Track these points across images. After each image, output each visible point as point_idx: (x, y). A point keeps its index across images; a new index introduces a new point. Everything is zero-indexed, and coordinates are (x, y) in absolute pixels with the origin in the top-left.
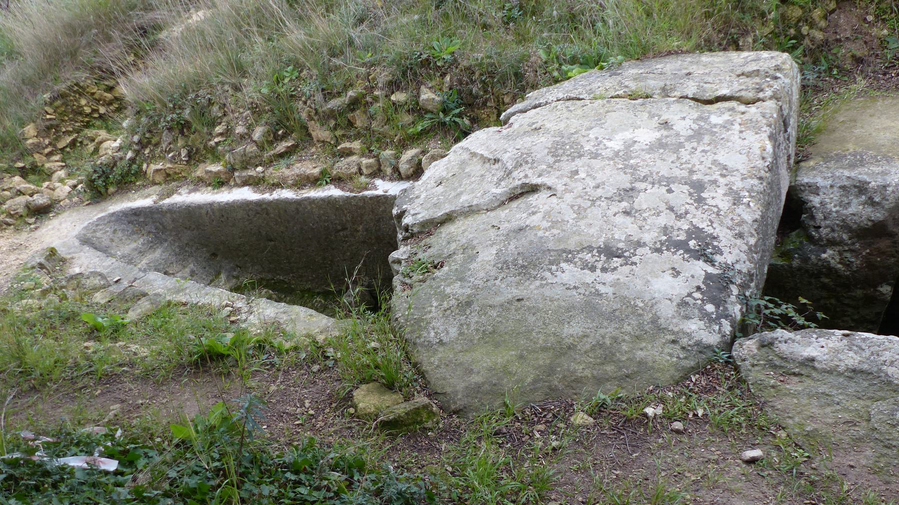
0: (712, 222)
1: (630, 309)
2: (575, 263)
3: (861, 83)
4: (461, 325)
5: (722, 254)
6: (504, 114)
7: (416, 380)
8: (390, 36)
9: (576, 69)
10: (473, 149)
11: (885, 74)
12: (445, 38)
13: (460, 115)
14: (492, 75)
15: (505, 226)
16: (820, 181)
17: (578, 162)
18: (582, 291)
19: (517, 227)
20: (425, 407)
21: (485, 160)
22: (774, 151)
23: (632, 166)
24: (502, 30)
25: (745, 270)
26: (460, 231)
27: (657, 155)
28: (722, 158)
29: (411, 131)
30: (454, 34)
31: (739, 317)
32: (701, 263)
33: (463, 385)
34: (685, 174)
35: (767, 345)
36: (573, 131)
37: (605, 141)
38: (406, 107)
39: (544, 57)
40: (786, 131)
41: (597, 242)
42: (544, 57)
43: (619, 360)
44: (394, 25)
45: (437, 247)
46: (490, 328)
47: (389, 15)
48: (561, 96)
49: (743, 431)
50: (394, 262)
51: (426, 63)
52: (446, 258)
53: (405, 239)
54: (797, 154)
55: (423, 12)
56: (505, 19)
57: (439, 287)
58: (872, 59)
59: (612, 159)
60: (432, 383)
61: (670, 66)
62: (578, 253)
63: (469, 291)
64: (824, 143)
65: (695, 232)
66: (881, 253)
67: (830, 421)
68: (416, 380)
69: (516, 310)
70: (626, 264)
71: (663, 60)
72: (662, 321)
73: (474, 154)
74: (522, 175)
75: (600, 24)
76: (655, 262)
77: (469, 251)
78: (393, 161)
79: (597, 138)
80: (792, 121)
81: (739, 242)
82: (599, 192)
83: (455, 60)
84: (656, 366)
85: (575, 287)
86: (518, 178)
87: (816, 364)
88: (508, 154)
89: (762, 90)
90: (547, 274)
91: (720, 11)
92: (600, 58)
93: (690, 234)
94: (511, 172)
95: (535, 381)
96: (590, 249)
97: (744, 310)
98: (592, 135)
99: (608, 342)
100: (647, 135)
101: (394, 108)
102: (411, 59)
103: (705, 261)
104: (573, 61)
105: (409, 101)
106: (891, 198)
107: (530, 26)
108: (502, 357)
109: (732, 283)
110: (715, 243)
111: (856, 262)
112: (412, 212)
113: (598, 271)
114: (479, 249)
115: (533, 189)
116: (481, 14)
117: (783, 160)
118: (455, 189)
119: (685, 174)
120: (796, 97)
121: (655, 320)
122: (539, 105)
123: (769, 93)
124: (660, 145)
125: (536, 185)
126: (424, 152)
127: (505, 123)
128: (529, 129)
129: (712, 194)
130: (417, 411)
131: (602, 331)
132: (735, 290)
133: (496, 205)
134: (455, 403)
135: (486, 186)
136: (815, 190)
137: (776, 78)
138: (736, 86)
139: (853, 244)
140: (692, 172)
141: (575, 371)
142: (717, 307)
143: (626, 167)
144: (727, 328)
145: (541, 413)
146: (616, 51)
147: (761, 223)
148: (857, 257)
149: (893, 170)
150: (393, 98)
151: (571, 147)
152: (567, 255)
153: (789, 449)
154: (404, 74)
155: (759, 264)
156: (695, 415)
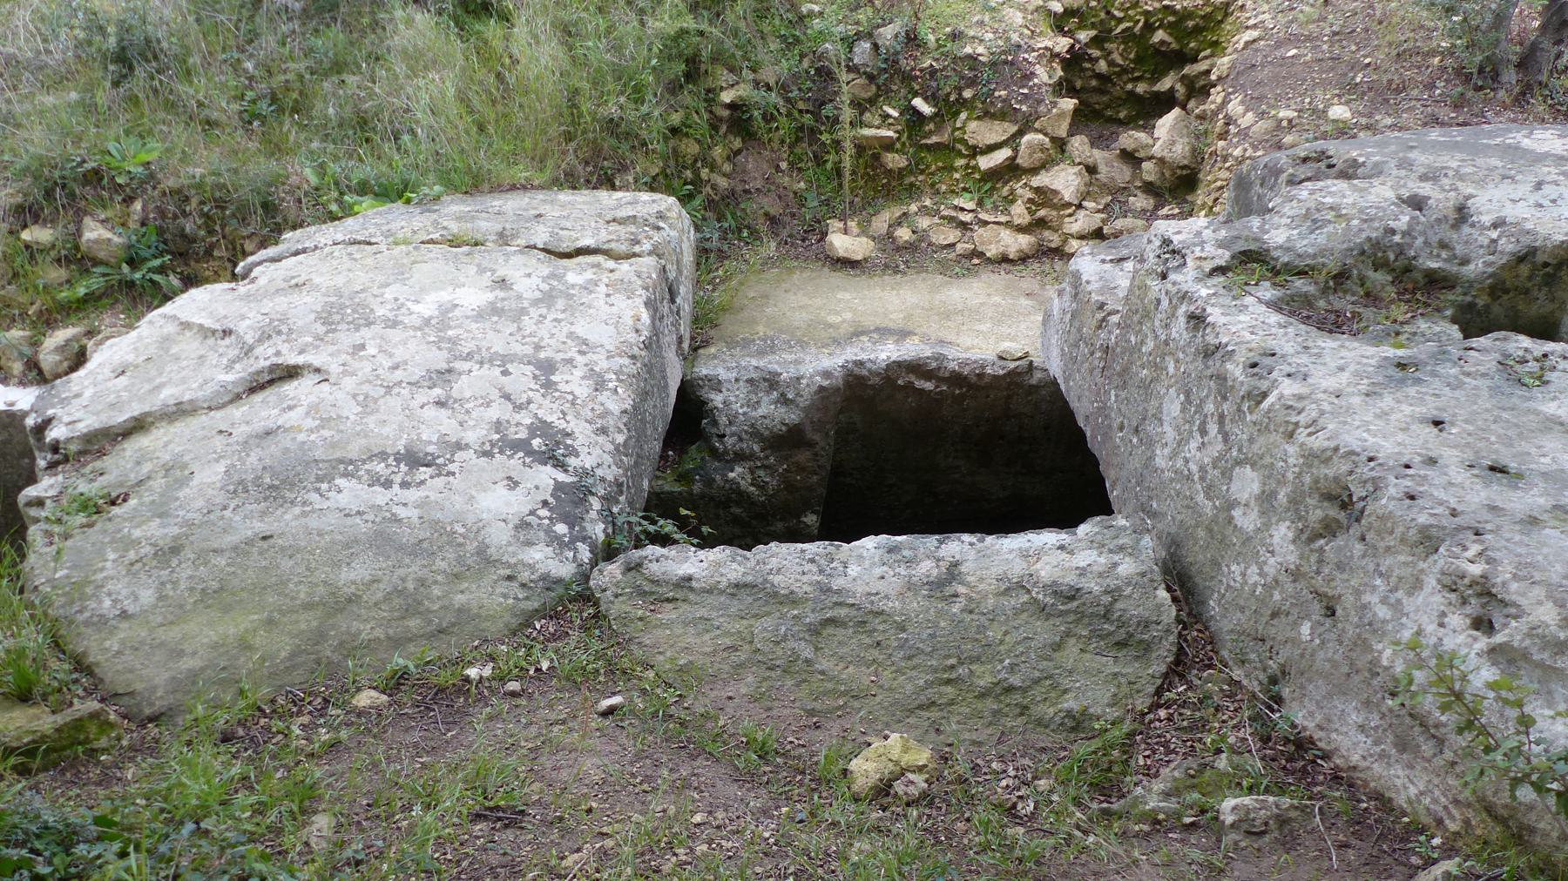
0: (564, 414)
1: (445, 538)
2: (359, 478)
3: (770, 247)
4: (163, 584)
5: (577, 456)
6: (242, 264)
7: (76, 681)
8: (18, 126)
9: (367, 201)
10: (184, 317)
12: (132, 139)
13: (162, 270)
14: (221, 204)
15: (241, 431)
16: (722, 374)
17: (364, 332)
18: (370, 517)
19: (261, 430)
20: (94, 716)
21: (206, 333)
22: (653, 322)
23: (450, 339)
24: (240, 132)
25: (610, 478)
26: (161, 443)
27: (488, 325)
28: (581, 329)
29: (64, 295)
30: (150, 132)
31: (602, 537)
32: (549, 469)
33: (167, 675)
34: (529, 350)
35: (633, 568)
36: (359, 288)
37: (409, 304)
38: (53, 253)
39: (314, 180)
40: (673, 301)
41: (393, 445)
42: (314, 180)
43: (429, 611)
44: (27, 106)
45: (115, 473)
46: (215, 585)
47: (15, 88)
48: (340, 237)
49: (602, 679)
50: (29, 504)
51: (94, 177)
52: (133, 486)
53: (52, 466)
54: (692, 338)
55: (85, 91)
56: (246, 116)
57: (120, 530)
58: (787, 219)
59: (420, 329)
60: (107, 680)
61: (512, 204)
62: (364, 462)
63: (176, 530)
64: (729, 325)
65: (541, 427)
66: (801, 469)
67: (708, 650)
68: (76, 681)
69: (260, 554)
70: (439, 475)
71: (504, 195)
72: (492, 551)
73: (186, 326)
74: (271, 351)
75: (406, 138)
76: (483, 470)
77: (177, 472)
78: (27, 350)
79: (396, 299)
80: (682, 290)
81: (601, 439)
82: (398, 375)
83: (152, 176)
84: (483, 612)
85: (358, 513)
86: (265, 357)
87: (694, 584)
88: (248, 322)
89: (638, 242)
90: (314, 497)
91: (584, 132)
92: (406, 187)
93: (532, 431)
94: (251, 349)
95: (293, 655)
96: (383, 456)
97: (610, 531)
98: (389, 294)
99: (411, 586)
100: (473, 296)
101: (27, 254)
102: (63, 168)
103: (555, 466)
104: (363, 189)
105: (59, 244)
106: (806, 393)
107: (289, 128)
108: (234, 627)
109: (591, 493)
110: (569, 442)
111: (773, 482)
112: (66, 419)
113: (396, 487)
114: (194, 467)
115: (291, 373)
116: (200, 104)
117: (669, 339)
118: (150, 380)
119: (529, 350)
120: (688, 258)
121: (482, 551)
122: (304, 251)
123: (647, 246)
124: (495, 310)
125: (296, 367)
126: (90, 334)
127: (244, 278)
128: (285, 285)
129: (566, 377)
130: (78, 724)
131: (401, 572)
132: (596, 504)
133: (226, 399)
134: (151, 704)
135: (207, 372)
136: (716, 384)
137: (659, 228)
138: (604, 236)
139: (767, 457)
140: (538, 347)
141: (360, 632)
142: (571, 527)
143: (441, 340)
144: (585, 554)
145: (303, 700)
146: (431, 177)
147: (635, 417)
148: (772, 475)
149: (808, 358)
150: (26, 235)
151: (354, 311)
152: (347, 467)
153: (659, 691)
154: (49, 194)
155: (634, 472)
156: (537, 670)
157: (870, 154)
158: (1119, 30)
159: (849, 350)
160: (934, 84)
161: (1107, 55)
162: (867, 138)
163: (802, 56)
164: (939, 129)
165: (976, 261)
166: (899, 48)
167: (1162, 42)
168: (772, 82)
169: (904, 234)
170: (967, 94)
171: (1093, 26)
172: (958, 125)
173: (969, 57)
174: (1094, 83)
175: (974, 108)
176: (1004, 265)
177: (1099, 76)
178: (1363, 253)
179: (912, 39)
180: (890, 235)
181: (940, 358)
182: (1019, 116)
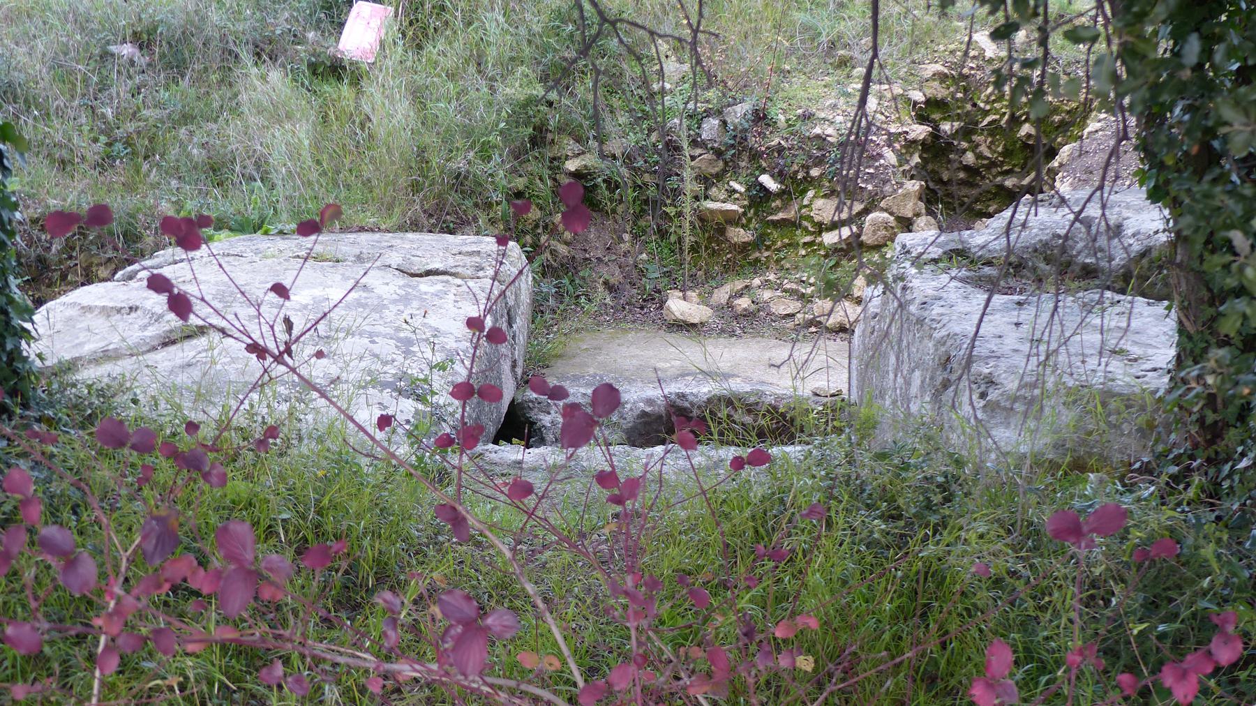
11: (642, 308)
73: (89, 309)
89: (482, 269)
133: (144, 349)
138: (451, 262)
157: (713, 229)
158: (985, 123)
159: (673, 385)
160: (781, 162)
161: (974, 147)
162: (712, 211)
163: (650, 130)
164: (784, 207)
165: (813, 329)
166: (746, 126)
167: (1029, 136)
168: (618, 153)
169: (744, 303)
170: (815, 172)
171: (959, 117)
172: (806, 202)
173: (818, 136)
174: (962, 175)
175: (821, 186)
176: (841, 335)
177: (967, 168)
178: (1036, 250)
179: (760, 117)
180: (729, 305)
181: (760, 394)
182: (865, 195)
